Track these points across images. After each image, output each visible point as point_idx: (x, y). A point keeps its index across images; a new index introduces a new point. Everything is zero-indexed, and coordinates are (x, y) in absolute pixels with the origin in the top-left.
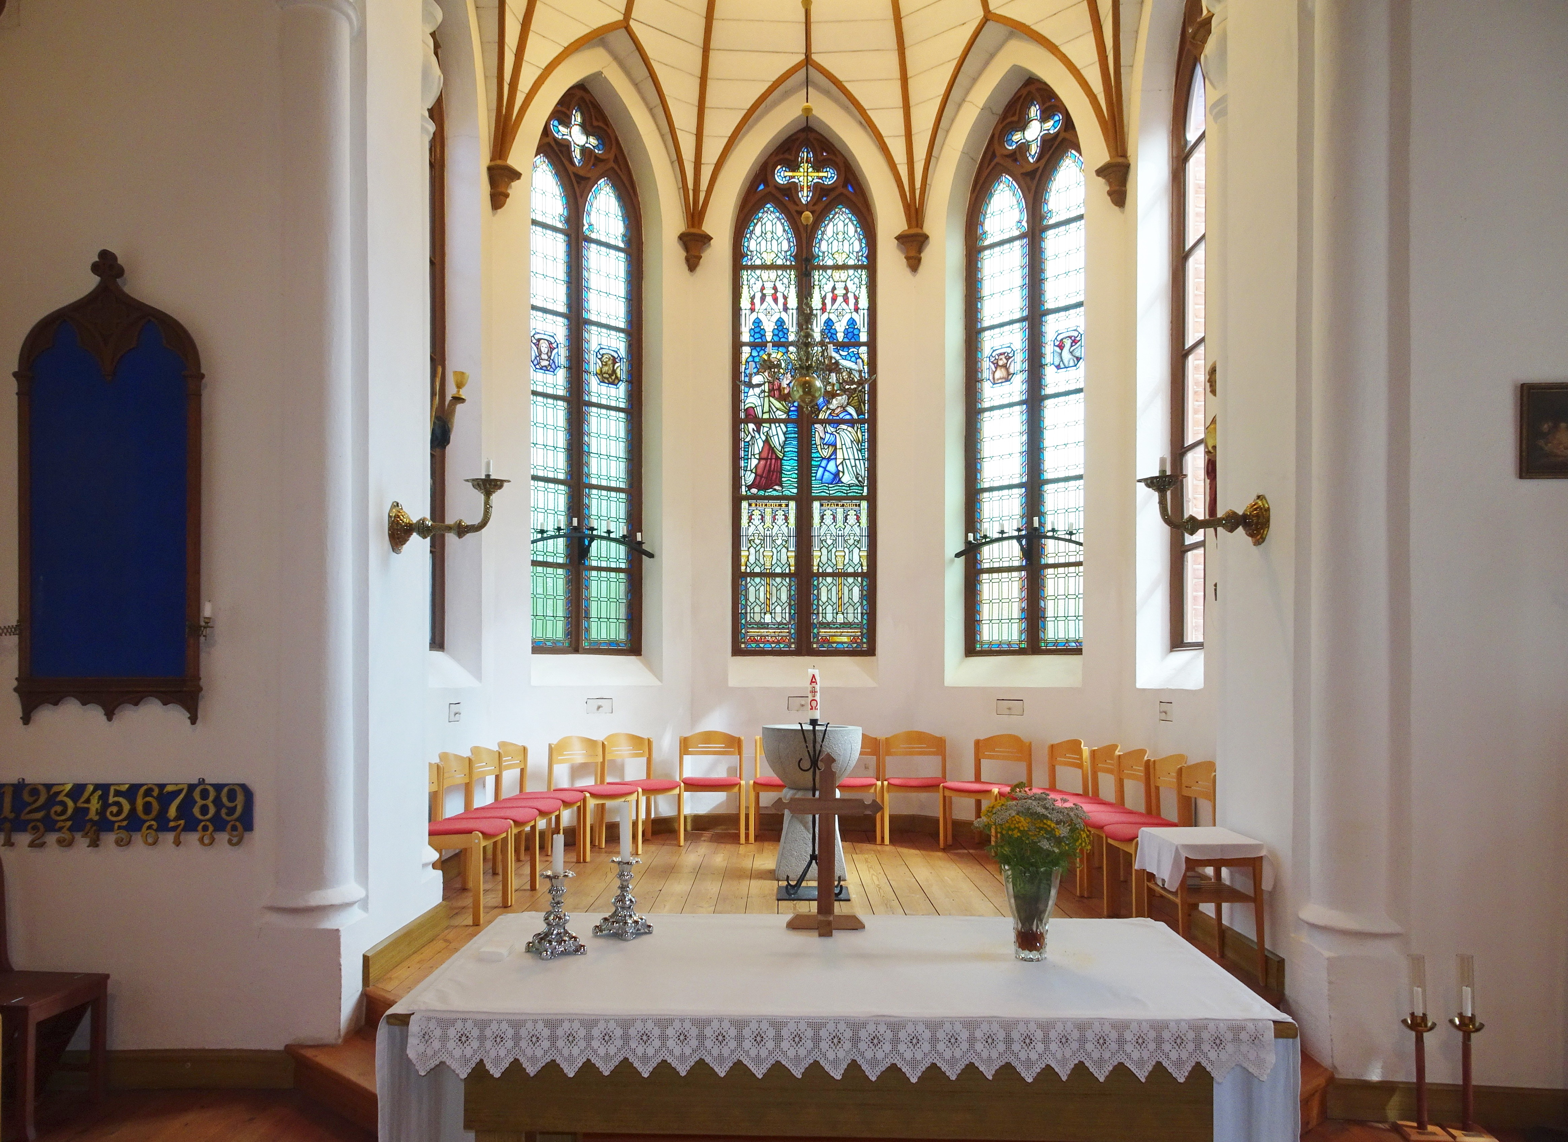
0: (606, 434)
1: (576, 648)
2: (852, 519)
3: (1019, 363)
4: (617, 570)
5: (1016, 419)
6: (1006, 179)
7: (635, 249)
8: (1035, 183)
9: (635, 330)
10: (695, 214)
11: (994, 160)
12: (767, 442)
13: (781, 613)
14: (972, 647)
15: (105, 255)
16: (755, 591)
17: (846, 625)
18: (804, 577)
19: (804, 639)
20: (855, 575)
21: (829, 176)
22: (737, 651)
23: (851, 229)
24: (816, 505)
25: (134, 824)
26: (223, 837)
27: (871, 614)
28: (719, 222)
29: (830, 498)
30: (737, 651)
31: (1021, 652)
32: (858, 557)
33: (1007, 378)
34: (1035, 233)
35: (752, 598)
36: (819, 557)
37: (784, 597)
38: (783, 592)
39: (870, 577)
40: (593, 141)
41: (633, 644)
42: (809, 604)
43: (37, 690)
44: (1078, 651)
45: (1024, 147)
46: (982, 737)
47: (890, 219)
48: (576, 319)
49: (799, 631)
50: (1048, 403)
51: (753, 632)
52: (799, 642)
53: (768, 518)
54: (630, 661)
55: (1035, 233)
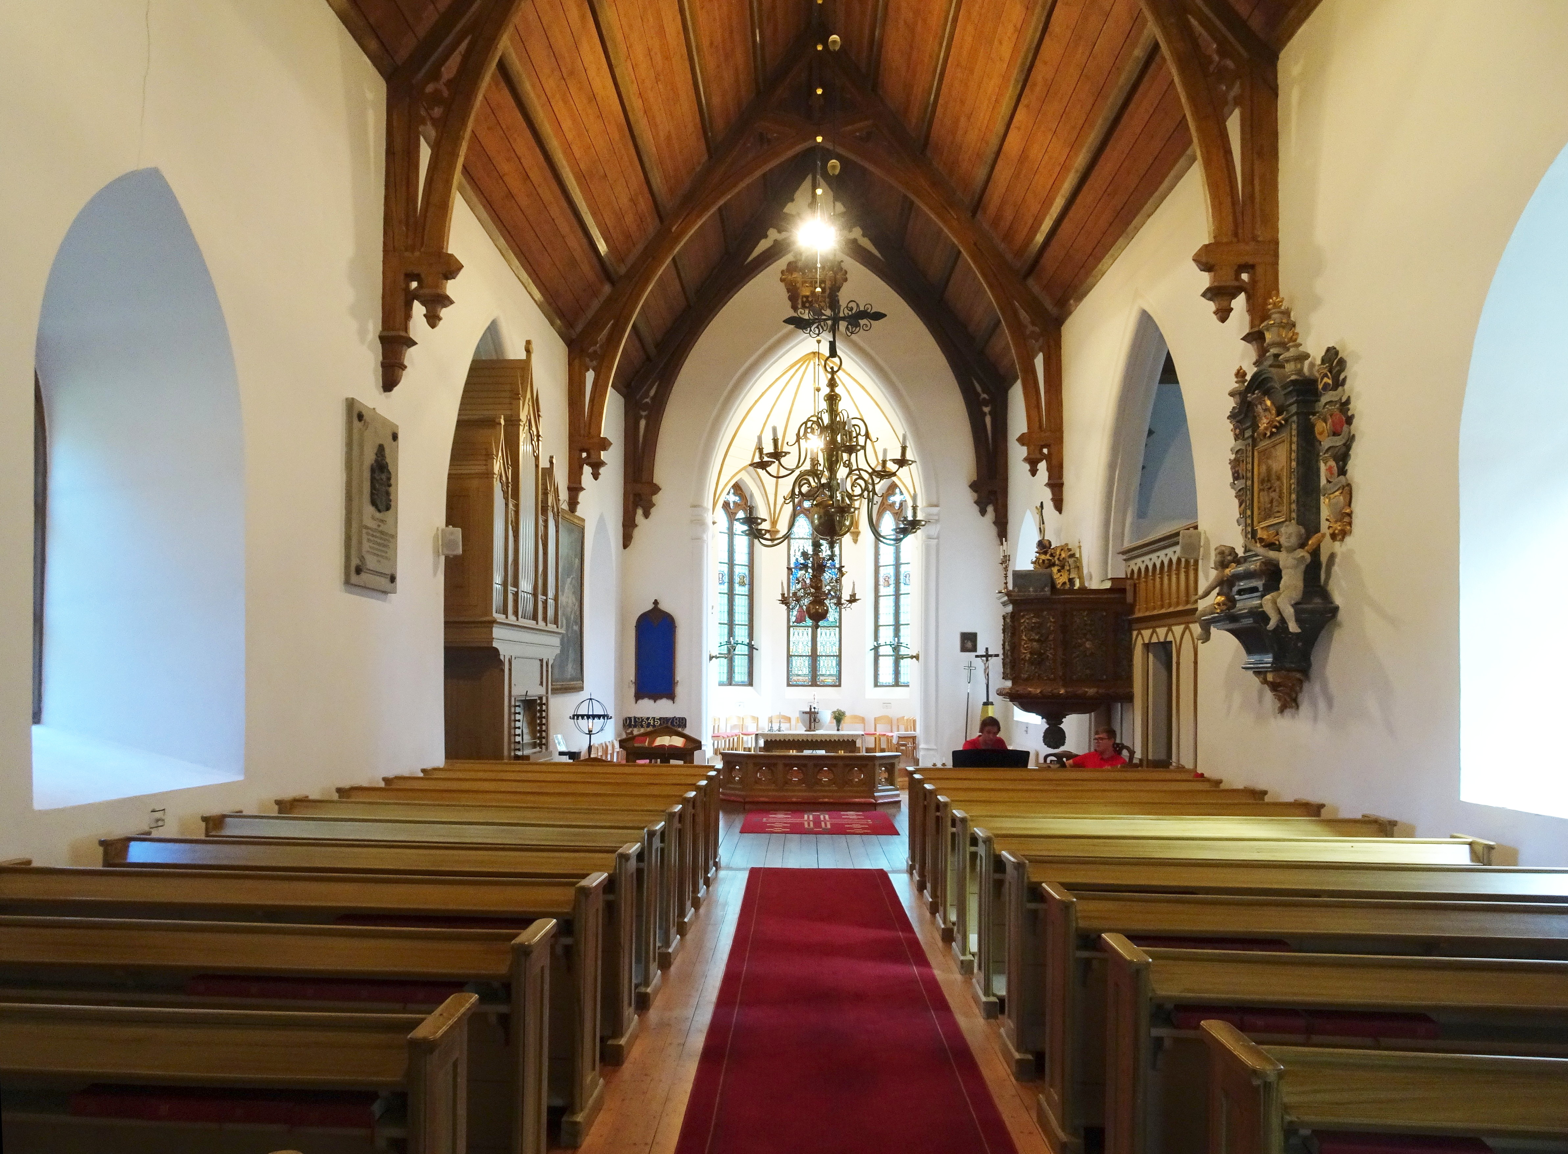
0: (741, 603)
2: (833, 634)
3: (892, 581)
6: (888, 512)
12: (905, 22)
13: (806, 670)
14: (876, 684)
16: (795, 661)
18: (814, 656)
19: (814, 681)
22: (789, 685)
27: (840, 672)
33: (889, 585)
36: (820, 650)
37: (807, 664)
39: (839, 656)
41: (751, 684)
42: (816, 667)
43: (638, 696)
44: (908, 686)
46: (877, 716)
48: (731, 564)
51: (795, 678)
54: (750, 688)
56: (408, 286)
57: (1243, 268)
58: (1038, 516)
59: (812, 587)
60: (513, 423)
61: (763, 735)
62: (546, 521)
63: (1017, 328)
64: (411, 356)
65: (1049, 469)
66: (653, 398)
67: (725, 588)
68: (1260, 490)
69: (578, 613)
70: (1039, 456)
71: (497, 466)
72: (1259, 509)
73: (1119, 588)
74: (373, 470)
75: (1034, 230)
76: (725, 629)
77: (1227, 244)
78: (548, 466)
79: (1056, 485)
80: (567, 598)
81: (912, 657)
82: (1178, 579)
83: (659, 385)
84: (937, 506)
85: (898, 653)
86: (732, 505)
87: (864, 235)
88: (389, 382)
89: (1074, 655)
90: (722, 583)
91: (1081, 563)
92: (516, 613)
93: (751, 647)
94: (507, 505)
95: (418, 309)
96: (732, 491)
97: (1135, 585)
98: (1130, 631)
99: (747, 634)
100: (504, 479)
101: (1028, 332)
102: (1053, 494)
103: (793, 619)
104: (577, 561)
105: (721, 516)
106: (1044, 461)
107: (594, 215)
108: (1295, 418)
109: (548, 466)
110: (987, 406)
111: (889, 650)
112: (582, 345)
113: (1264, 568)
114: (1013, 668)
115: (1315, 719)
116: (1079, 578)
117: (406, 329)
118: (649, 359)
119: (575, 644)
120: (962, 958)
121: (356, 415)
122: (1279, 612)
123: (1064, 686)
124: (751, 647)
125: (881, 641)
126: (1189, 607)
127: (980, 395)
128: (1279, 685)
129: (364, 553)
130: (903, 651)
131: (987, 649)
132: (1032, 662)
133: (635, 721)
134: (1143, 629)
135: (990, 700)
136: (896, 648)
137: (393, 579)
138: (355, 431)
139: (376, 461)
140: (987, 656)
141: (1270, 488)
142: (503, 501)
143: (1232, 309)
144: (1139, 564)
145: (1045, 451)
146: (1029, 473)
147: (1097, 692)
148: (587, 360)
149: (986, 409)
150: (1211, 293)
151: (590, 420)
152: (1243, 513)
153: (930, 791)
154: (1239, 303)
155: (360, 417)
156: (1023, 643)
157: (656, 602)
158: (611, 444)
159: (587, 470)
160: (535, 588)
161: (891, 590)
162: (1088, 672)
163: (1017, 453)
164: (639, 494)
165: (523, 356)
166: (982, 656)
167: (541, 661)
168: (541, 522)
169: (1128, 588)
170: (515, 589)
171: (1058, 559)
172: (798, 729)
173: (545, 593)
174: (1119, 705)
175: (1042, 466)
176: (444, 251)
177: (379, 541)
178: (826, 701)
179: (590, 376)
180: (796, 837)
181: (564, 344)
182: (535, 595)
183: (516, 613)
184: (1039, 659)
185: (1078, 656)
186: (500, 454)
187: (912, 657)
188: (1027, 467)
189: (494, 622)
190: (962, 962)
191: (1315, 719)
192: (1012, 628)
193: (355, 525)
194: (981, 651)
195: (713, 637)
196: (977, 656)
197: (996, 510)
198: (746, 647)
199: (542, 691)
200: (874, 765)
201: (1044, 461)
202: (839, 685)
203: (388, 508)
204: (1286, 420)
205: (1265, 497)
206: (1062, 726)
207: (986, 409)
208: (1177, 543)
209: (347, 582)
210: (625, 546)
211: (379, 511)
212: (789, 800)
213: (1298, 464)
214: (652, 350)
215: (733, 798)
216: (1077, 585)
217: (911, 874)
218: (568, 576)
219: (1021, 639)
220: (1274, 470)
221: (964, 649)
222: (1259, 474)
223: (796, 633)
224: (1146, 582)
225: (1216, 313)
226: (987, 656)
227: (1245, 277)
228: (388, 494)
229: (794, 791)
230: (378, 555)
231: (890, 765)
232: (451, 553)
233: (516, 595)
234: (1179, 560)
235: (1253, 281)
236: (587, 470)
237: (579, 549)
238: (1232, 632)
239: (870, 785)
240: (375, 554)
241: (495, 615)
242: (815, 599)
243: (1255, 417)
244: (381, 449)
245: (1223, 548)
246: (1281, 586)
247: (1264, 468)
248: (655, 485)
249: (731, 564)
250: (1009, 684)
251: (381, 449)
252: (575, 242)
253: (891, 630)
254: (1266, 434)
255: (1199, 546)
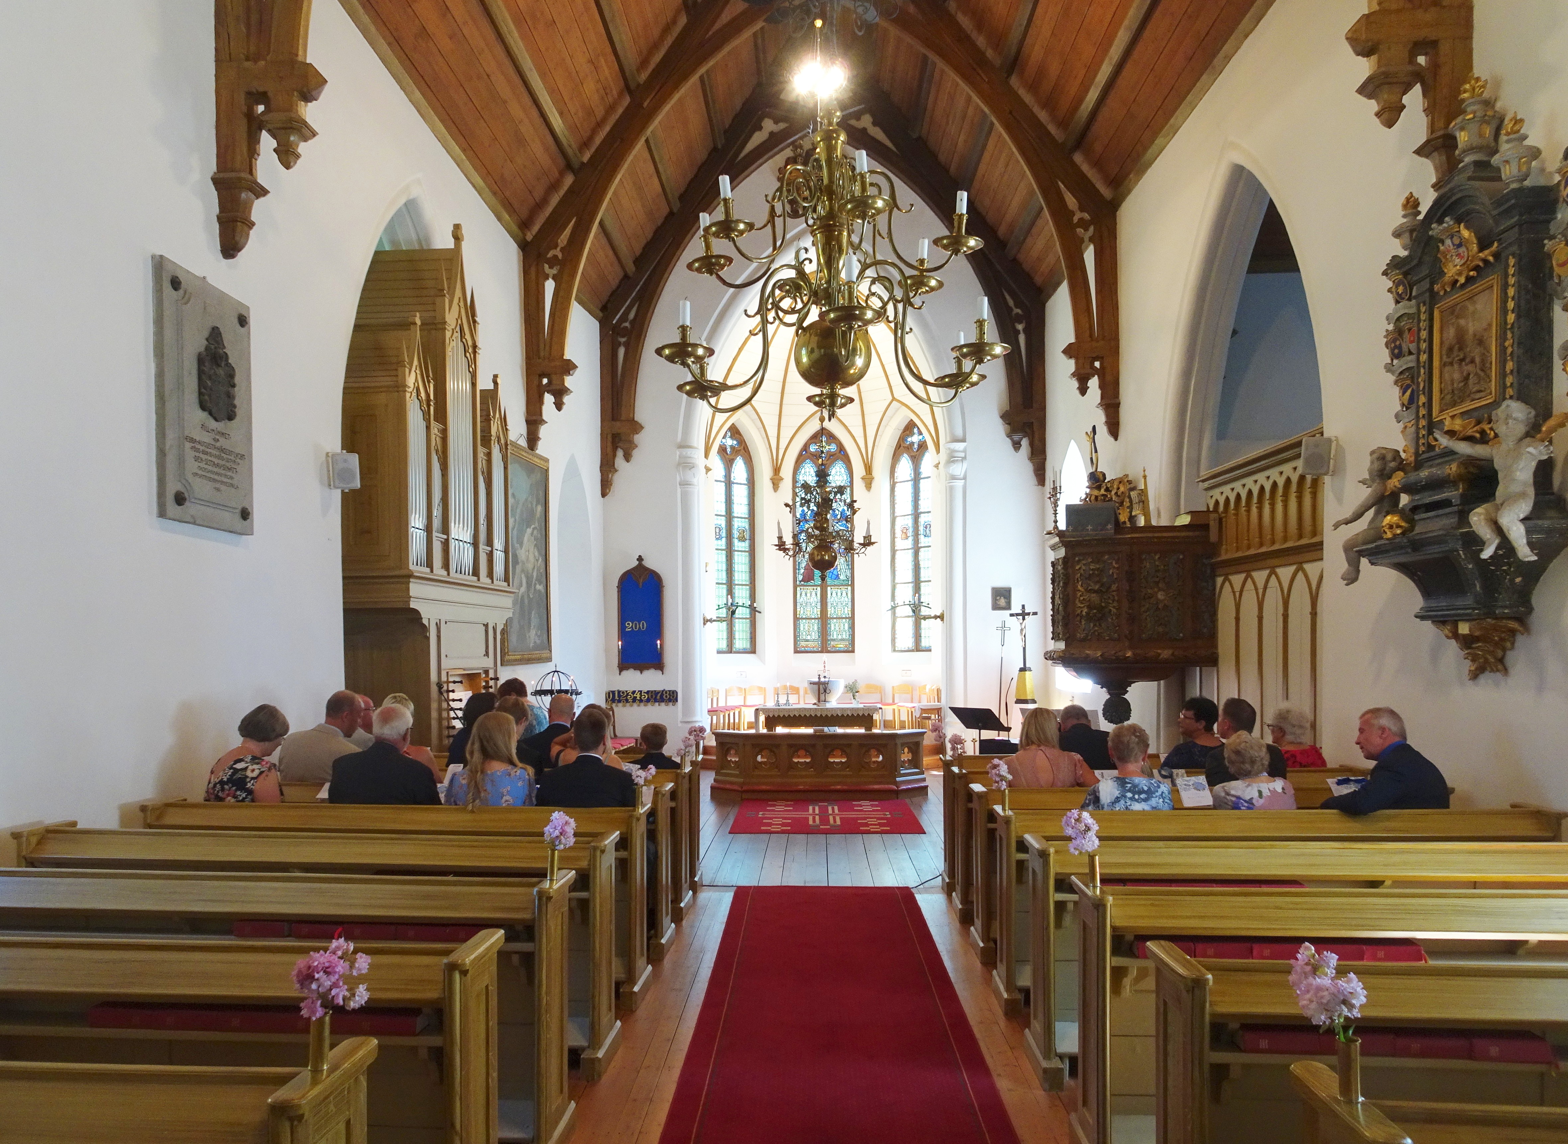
0: (741, 561)
1: (731, 652)
2: (844, 594)
4: (746, 618)
5: (910, 554)
7: (751, 483)
8: (916, 460)
9: (752, 517)
10: (777, 470)
11: (902, 447)
13: (815, 635)
15: (640, 556)
16: (803, 625)
17: (842, 640)
18: (824, 619)
20: (846, 618)
21: (833, 448)
23: (843, 470)
24: (829, 588)
25: (648, 701)
26: (671, 704)
28: (787, 472)
29: (835, 585)
30: (796, 652)
31: (913, 651)
32: (847, 611)
33: (907, 538)
34: (916, 479)
35: (802, 629)
36: (830, 611)
37: (816, 628)
38: (815, 626)
39: (852, 618)
40: (735, 442)
41: (753, 651)
44: (930, 650)
45: (912, 443)
47: (859, 470)
48: (729, 516)
49: (822, 643)
50: (922, 550)
51: (803, 644)
52: (822, 647)
53: (808, 595)
55: (916, 479)
56: (541, 382)
57: (1418, 47)
58: (1088, 445)
59: (817, 528)
60: (435, 326)
61: (765, 711)
62: (489, 455)
63: (1061, 214)
64: (259, 209)
65: (1102, 386)
66: (633, 322)
67: (723, 543)
68: (1443, 365)
69: (543, 570)
70: (1090, 371)
71: (412, 379)
72: (1441, 391)
73: (1200, 523)
74: (200, 360)
75: (1080, 100)
76: (724, 589)
77: (1398, 11)
78: (491, 386)
79: (1111, 405)
80: (527, 553)
81: (936, 617)
82: (1273, 510)
83: (639, 305)
84: (963, 440)
85: (941, 599)
86: (729, 450)
87: (875, 124)
88: (230, 247)
89: (1143, 609)
90: (719, 538)
91: (1146, 496)
92: (446, 566)
93: (753, 610)
94: (428, 428)
95: (267, 142)
96: (729, 434)
97: (1220, 520)
98: (1213, 577)
99: (748, 595)
100: (423, 394)
101: (1075, 219)
102: (1107, 416)
103: (800, 577)
104: (540, 509)
105: (716, 463)
106: (1096, 377)
107: (543, 75)
108: (1514, 248)
109: (491, 386)
110: (1020, 323)
111: (908, 611)
112: (541, 250)
113: (1463, 470)
114: (1065, 625)
115: (1540, 688)
116: (1144, 515)
117: (251, 170)
118: (626, 276)
119: (537, 606)
120: (1045, 1064)
121: (169, 281)
122: (1499, 531)
123: (1131, 648)
124: (753, 610)
125: (899, 600)
126: (1314, 540)
127: (1012, 310)
128: (1477, 639)
129: (190, 477)
130: (924, 611)
131: (1023, 606)
132: (1089, 618)
133: (619, 696)
134: (1277, 566)
135: (1027, 666)
136: (916, 608)
137: (245, 514)
138: (166, 304)
139: (207, 349)
140: (1024, 614)
141: (1462, 360)
142: (423, 424)
143: (1404, 107)
144: (1227, 492)
145: (1097, 364)
146: (1077, 392)
147: (1173, 654)
148: (546, 266)
149: (1020, 327)
150: (1367, 89)
151: (551, 339)
152: (1410, 404)
153: (980, 795)
154: (1414, 98)
155: (176, 284)
156: (1079, 594)
157: (640, 559)
158: (575, 367)
159: (549, 399)
160: (476, 536)
161: (909, 543)
162: (1161, 629)
163: (1060, 370)
164: (618, 432)
165: (450, 244)
166: (1017, 615)
167: (486, 626)
168: (481, 455)
169: (1212, 523)
170: (490, 549)
171: (1116, 493)
172: (806, 702)
173: (490, 542)
174: (1198, 668)
175: (1094, 383)
176: (300, 58)
177: (216, 461)
178: (838, 669)
179: (550, 286)
180: (802, 837)
181: (516, 245)
182: (475, 544)
183: (446, 566)
184: (1098, 614)
185: (1148, 610)
186: (416, 362)
187: (936, 617)
188: (1075, 384)
189: (410, 576)
190: (1045, 1071)
191: (1540, 688)
192: (1064, 578)
193: (171, 436)
194: (1016, 608)
195: (708, 596)
196: (1012, 615)
197: (1032, 444)
198: (748, 610)
199: (488, 663)
200: (896, 744)
201: (1096, 377)
202: (853, 651)
203: (231, 417)
204: (1497, 255)
205: (1455, 374)
206: (1126, 696)
207: (1020, 327)
208: (1298, 456)
209: (162, 513)
210: (604, 495)
211: (216, 420)
212: (795, 788)
213: (1518, 317)
214: (631, 268)
215: (728, 786)
216: (1141, 522)
217: (949, 895)
218: (528, 526)
219: (1075, 590)
220: (1471, 332)
221: (996, 607)
222: (1442, 343)
223: (803, 594)
224: (1237, 515)
225: (1378, 115)
226: (1024, 614)
227: (1421, 60)
228: (230, 397)
229: (802, 777)
230: (214, 480)
231: (914, 743)
232: (348, 487)
233: (446, 544)
234: (1302, 478)
235: (1435, 66)
236: (549, 399)
237: (541, 494)
238: (1401, 567)
239: (891, 767)
240: (210, 479)
241: (412, 567)
242: (823, 547)
243: (1437, 260)
244: (215, 335)
245: (1384, 452)
246: (1497, 493)
247: (1451, 332)
248: (637, 423)
249: (729, 516)
250: (1061, 645)
251: (215, 335)
252: (529, 129)
253: (910, 588)
254: (1456, 281)
255: (1329, 458)
